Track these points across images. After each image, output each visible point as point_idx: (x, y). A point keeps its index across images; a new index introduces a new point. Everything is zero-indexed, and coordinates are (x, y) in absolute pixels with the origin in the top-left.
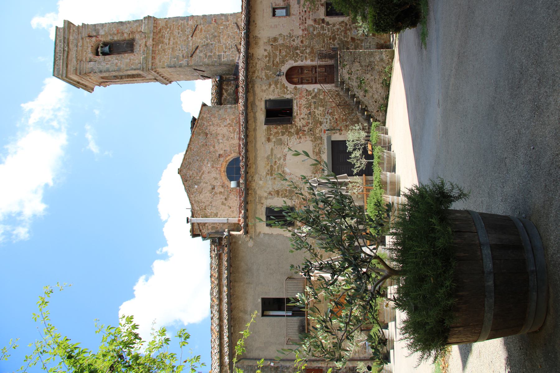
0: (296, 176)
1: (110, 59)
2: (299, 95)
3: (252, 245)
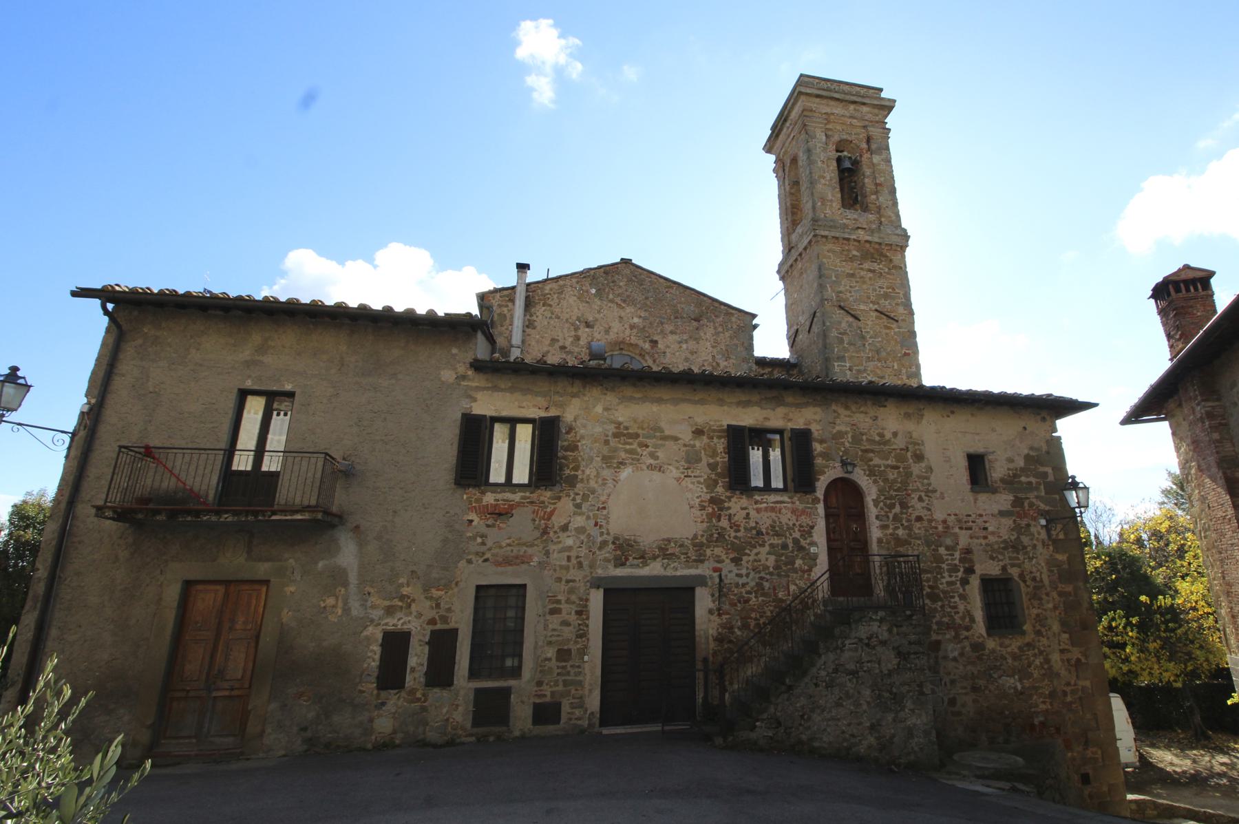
0: (609, 495)
1: (831, 168)
2: (800, 508)
3: (443, 379)
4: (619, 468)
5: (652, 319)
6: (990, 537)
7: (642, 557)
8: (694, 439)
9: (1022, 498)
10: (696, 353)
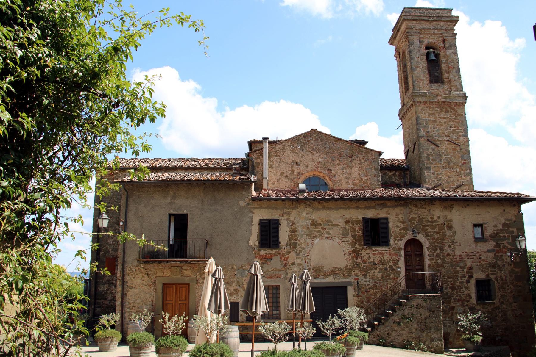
0: (310, 250)
1: (423, 61)
4: (314, 239)
5: (328, 158)
6: (482, 262)
7: (325, 275)
8: (346, 224)
9: (499, 244)
10: (351, 174)
